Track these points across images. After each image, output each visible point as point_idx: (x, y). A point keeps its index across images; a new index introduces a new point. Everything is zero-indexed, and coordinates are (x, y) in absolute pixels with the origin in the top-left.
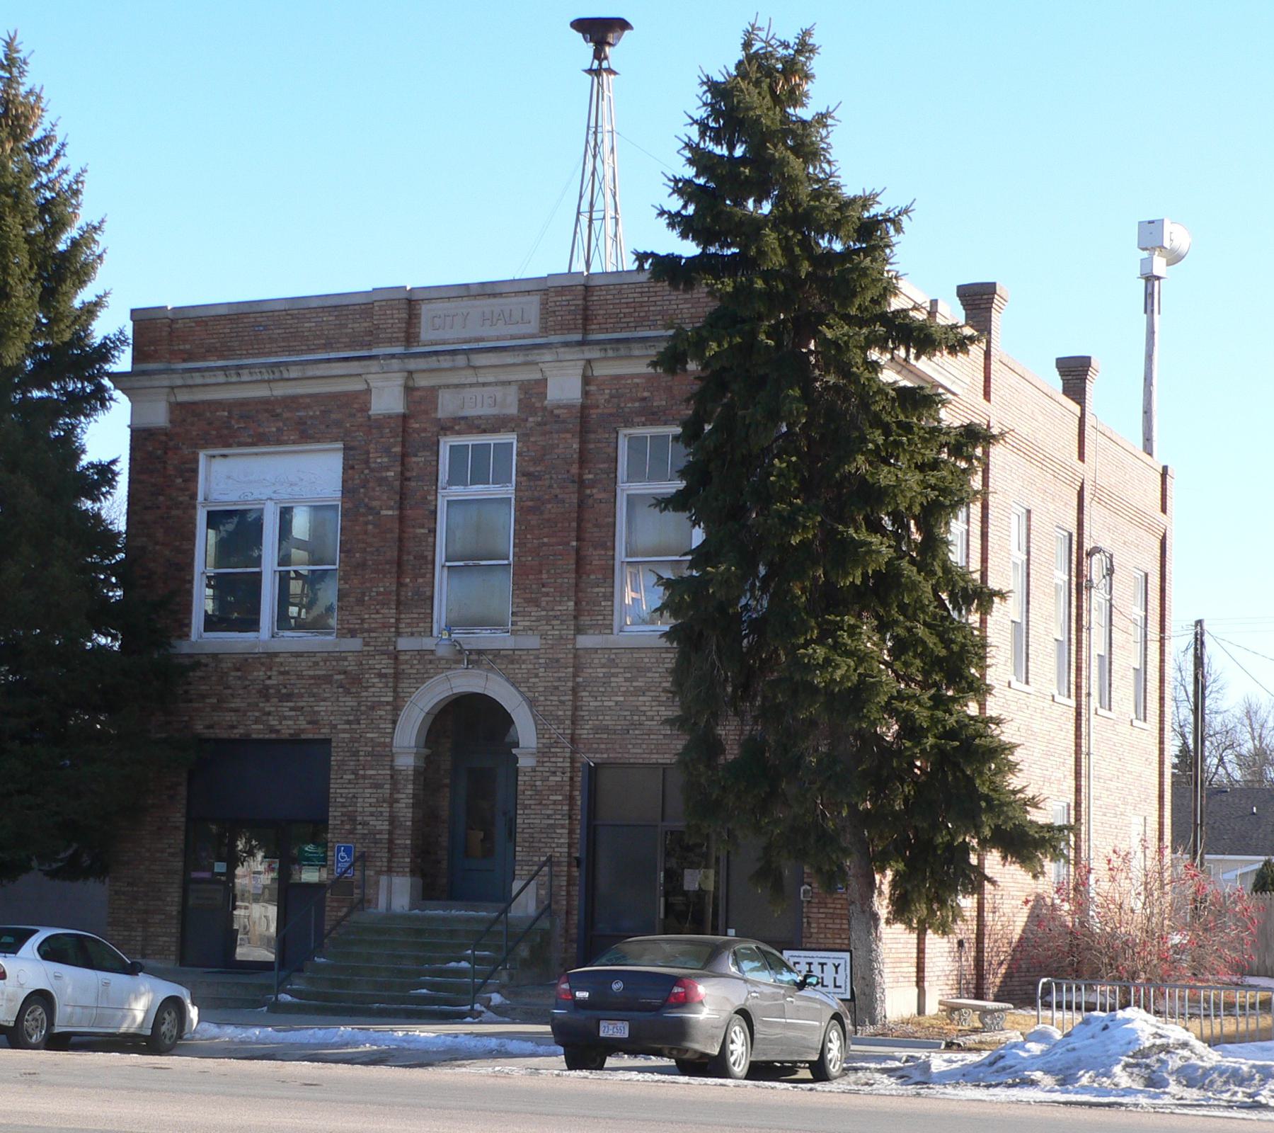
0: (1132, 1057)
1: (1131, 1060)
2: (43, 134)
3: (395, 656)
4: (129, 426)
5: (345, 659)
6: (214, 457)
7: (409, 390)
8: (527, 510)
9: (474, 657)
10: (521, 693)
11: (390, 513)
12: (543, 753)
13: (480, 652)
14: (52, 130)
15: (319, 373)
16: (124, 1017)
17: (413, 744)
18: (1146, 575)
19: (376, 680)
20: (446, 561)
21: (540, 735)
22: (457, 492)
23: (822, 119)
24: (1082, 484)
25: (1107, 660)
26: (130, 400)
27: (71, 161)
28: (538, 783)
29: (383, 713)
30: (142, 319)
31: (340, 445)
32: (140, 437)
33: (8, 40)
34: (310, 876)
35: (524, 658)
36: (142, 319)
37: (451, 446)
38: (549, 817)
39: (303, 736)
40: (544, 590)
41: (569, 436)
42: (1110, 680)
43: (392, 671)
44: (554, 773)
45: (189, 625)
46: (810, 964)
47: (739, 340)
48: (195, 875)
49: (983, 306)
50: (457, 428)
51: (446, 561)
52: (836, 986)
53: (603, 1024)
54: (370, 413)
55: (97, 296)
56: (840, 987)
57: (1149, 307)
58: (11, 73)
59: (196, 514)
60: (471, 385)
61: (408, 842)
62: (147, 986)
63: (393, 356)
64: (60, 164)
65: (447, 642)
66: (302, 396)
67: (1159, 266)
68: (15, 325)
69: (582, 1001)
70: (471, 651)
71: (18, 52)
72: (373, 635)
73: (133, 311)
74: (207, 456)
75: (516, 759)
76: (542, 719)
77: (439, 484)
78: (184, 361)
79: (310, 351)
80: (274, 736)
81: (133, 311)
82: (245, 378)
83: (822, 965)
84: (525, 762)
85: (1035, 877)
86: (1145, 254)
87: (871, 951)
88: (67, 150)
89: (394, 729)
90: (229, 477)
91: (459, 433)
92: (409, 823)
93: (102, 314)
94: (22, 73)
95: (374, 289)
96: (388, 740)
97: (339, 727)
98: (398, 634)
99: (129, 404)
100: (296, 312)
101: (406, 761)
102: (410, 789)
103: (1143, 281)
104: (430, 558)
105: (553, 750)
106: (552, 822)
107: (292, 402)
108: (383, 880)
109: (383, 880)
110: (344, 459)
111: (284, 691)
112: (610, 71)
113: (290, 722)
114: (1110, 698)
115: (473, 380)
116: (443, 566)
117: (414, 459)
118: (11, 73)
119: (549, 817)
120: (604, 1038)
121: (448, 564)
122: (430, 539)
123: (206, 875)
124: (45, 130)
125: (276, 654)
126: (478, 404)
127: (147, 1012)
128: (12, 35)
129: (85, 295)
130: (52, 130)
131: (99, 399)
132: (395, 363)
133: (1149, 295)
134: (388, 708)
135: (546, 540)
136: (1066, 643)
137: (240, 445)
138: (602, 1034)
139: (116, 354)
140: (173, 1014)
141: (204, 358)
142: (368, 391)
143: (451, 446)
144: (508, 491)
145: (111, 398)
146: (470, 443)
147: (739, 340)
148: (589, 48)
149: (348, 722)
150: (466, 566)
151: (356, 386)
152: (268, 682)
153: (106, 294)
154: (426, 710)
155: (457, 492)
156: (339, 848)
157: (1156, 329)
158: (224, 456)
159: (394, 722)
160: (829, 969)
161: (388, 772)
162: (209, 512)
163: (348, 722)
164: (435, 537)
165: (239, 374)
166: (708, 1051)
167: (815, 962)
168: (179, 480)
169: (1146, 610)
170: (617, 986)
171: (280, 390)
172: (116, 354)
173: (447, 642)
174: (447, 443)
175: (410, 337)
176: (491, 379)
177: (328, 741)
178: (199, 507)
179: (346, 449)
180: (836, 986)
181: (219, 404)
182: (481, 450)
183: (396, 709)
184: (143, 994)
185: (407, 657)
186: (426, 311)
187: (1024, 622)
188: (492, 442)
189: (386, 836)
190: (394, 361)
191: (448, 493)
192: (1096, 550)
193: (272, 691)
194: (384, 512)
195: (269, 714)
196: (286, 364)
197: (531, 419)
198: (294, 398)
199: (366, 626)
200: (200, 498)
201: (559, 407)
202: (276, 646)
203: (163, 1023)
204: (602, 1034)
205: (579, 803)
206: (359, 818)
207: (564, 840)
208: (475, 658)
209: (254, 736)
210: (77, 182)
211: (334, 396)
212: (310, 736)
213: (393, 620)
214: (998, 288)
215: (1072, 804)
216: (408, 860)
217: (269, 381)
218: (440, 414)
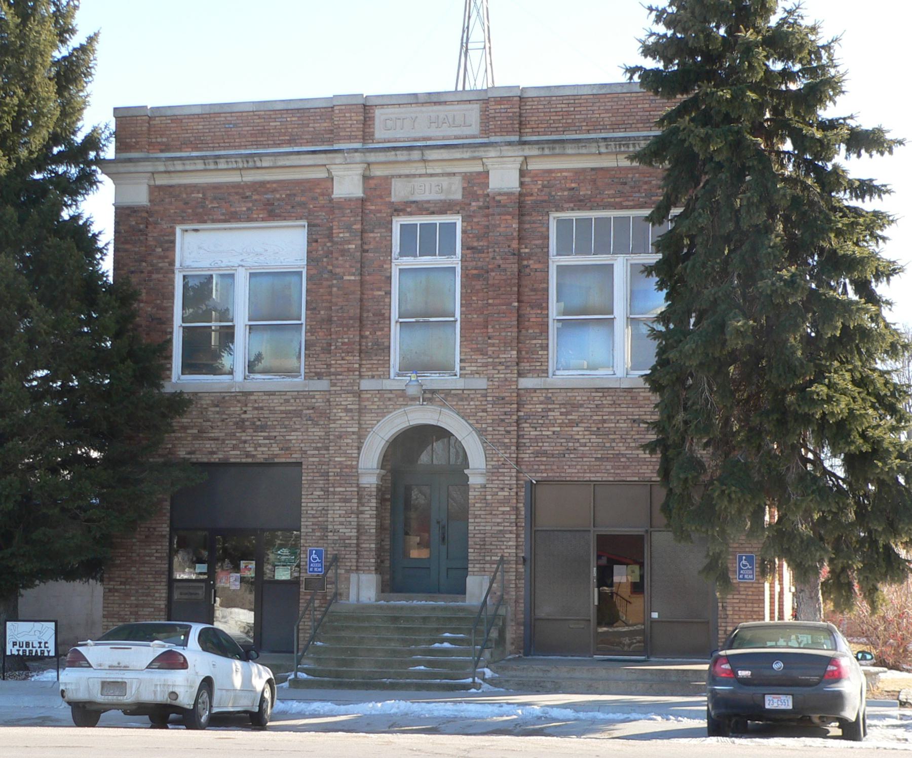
3: (359, 394)
4: (113, 205)
6: (187, 231)
12: (493, 472)
13: (433, 392)
35: (472, 396)
36: (124, 117)
37: (401, 225)
51: (399, 318)
60: (420, 176)
61: (373, 546)
73: (115, 109)
79: (279, 145)
82: (222, 165)
89: (359, 454)
90: (200, 248)
98: (361, 376)
99: (113, 186)
104: (387, 315)
105: (500, 470)
107: (260, 187)
108: (353, 577)
116: (397, 322)
119: (498, 524)
132: (358, 157)
134: (354, 437)
137: (214, 221)
143: (401, 225)
146: (418, 223)
158: (196, 230)
165: (216, 163)
173: (416, 383)
174: (398, 222)
175: (366, 134)
176: (439, 171)
178: (176, 272)
181: (195, 188)
186: (378, 113)
188: (438, 222)
194: (346, 278)
195: (245, 442)
196: (260, 155)
198: (263, 184)
200: (177, 264)
201: (500, 194)
202: (250, 386)
211: (298, 183)
218: (393, 199)
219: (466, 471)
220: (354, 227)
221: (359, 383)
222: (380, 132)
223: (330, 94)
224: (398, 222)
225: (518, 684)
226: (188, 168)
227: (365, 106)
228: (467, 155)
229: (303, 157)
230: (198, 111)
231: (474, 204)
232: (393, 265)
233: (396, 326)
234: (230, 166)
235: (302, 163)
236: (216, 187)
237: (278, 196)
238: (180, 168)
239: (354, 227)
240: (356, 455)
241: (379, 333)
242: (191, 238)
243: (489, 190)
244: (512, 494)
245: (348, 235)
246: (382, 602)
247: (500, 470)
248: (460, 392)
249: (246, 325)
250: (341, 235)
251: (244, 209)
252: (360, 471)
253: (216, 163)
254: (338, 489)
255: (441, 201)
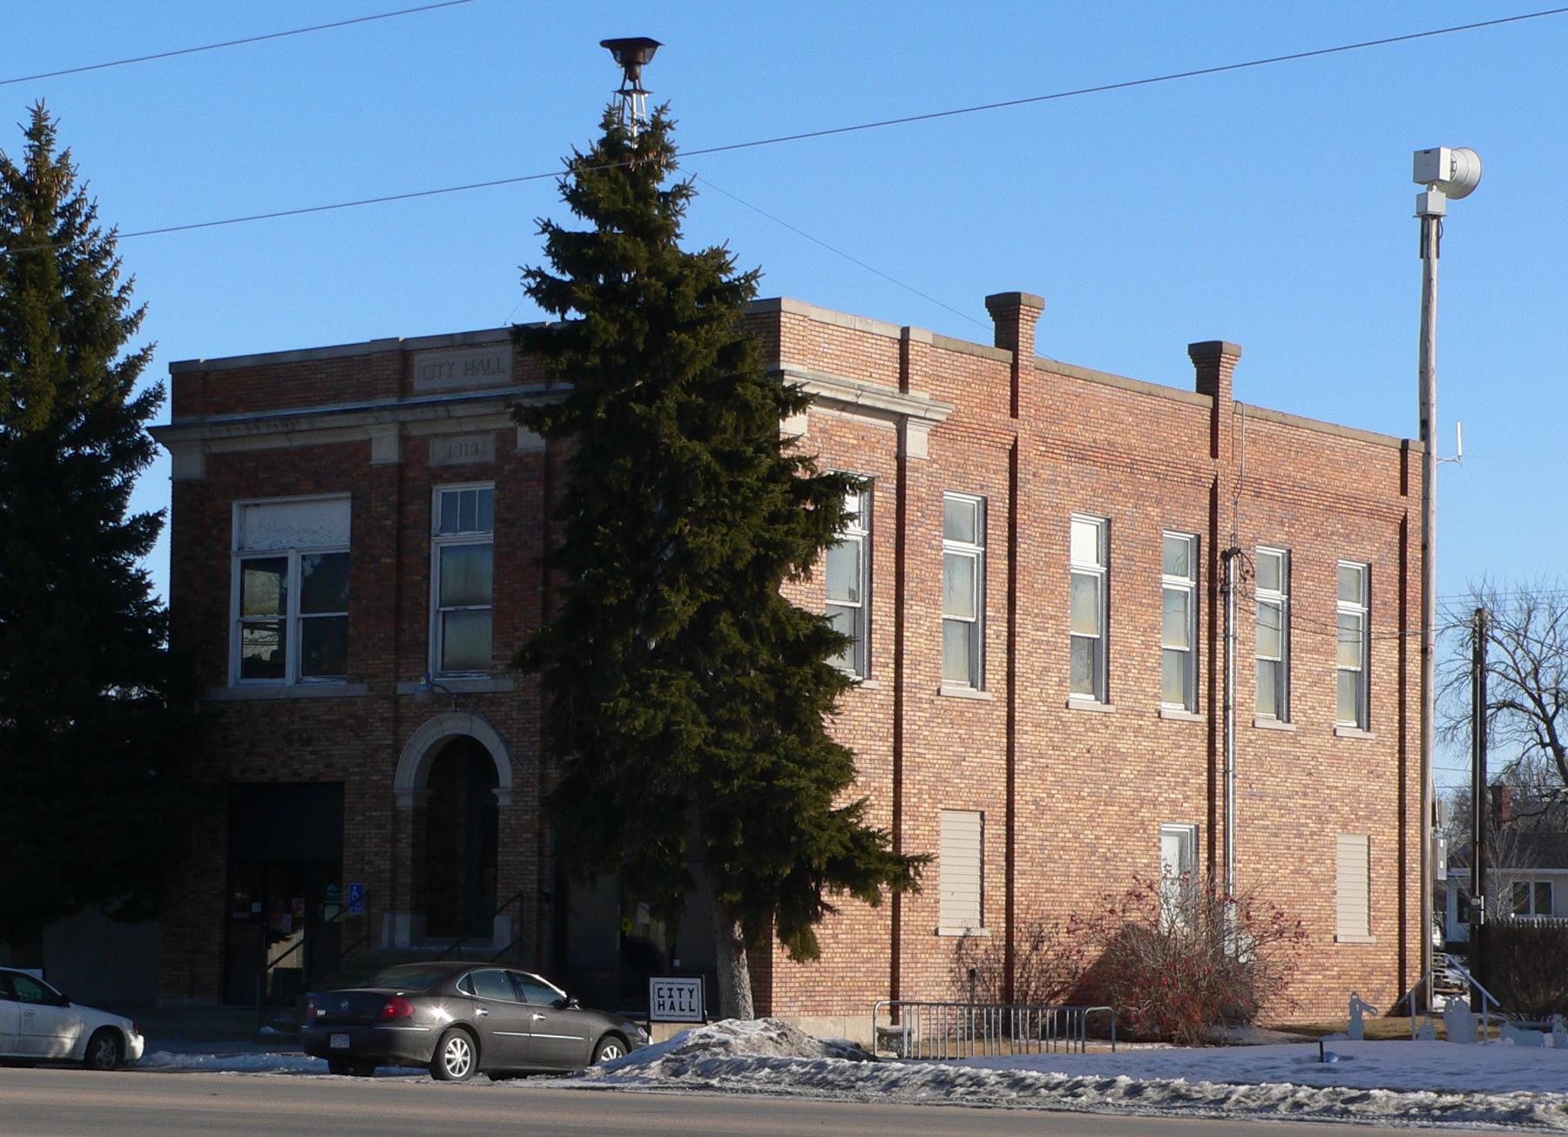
0: (674, 1054)
1: (672, 1056)
2: (74, 198)
3: (396, 700)
4: (170, 478)
5: (354, 704)
6: (247, 506)
7: (404, 439)
8: (503, 554)
9: (461, 700)
10: (500, 735)
11: (388, 560)
12: (517, 792)
13: (467, 695)
14: (82, 194)
15: (325, 425)
16: (50, 1044)
17: (412, 785)
18: (1370, 566)
19: (378, 724)
20: (440, 606)
21: (515, 776)
22: (448, 539)
23: (681, 191)
24: (1216, 480)
25: (1285, 666)
26: (171, 453)
27: (102, 224)
28: (513, 822)
29: (385, 756)
30: (180, 371)
31: (349, 494)
32: (181, 488)
33: (36, 109)
34: (330, 913)
35: (502, 700)
36: (180, 371)
37: (443, 494)
38: (522, 854)
39: (322, 779)
40: (516, 634)
41: (535, 483)
42: (1289, 688)
43: (391, 715)
44: (526, 812)
45: (226, 672)
46: (671, 990)
47: (578, 413)
48: (236, 915)
49: (1011, 317)
50: (445, 476)
51: (440, 606)
52: (691, 1010)
53: (333, 1037)
54: (371, 463)
55: (142, 350)
56: (694, 1010)
57: (1425, 253)
58: (40, 141)
59: (230, 563)
60: (457, 434)
61: (409, 880)
62: (78, 1018)
63: (384, 408)
64: (91, 227)
65: (424, 688)
66: (318, 447)
67: (1437, 202)
68: (34, 394)
69: (321, 1017)
70: (458, 694)
71: (46, 120)
72: (376, 680)
73: (171, 365)
74: (240, 506)
75: (496, 799)
76: (515, 759)
77: (433, 531)
78: (218, 413)
79: (323, 402)
80: (297, 780)
81: (171, 365)
82: (264, 430)
83: (680, 990)
84: (504, 801)
85: (874, 905)
86: (1423, 188)
87: (733, 977)
88: (98, 212)
89: (395, 771)
90: (261, 526)
91: (447, 481)
92: (409, 863)
93: (147, 367)
94: (49, 142)
95: (372, 341)
96: (389, 782)
97: (351, 770)
98: (398, 679)
99: (170, 456)
100: (309, 363)
101: (406, 803)
102: (409, 829)
103: (1419, 220)
104: (424, 604)
105: (525, 790)
106: (524, 859)
107: (307, 452)
108: (387, 917)
109: (387, 917)
110: (352, 507)
111: (305, 735)
112: (642, 92)
113: (310, 766)
114: (1289, 708)
115: (458, 429)
116: (438, 612)
117: (410, 508)
118: (40, 141)
119: (522, 854)
120: (334, 1049)
121: (442, 609)
122: (424, 586)
123: (245, 915)
124: (75, 194)
125: (296, 700)
126: (461, 452)
127: (78, 1041)
128: (40, 104)
129: (126, 350)
130: (82, 194)
131: (142, 453)
132: (387, 415)
133: (1425, 237)
134: (389, 751)
135: (517, 586)
136: (1194, 654)
137: (266, 495)
138: (332, 1045)
139: (153, 409)
140: (111, 1043)
141: (232, 410)
142: (369, 442)
143: (443, 494)
144: (488, 538)
145: (156, 452)
146: (459, 490)
147: (578, 413)
148: (621, 71)
149: (359, 765)
150: (457, 610)
151: (357, 436)
152: (293, 727)
153: (150, 348)
154: (423, 751)
155: (448, 539)
156: (352, 887)
157: (1434, 276)
158: (257, 505)
159: (395, 764)
160: (686, 994)
161: (390, 813)
162: (242, 561)
163: (359, 765)
164: (429, 583)
165: (258, 428)
166: (424, 1060)
167: (675, 987)
168: (215, 531)
169: (1370, 606)
170: (345, 1004)
171: (298, 442)
172: (153, 409)
173: (424, 688)
174: (439, 491)
175: (404, 388)
176: (472, 428)
177: (340, 785)
178: (233, 557)
179: (354, 499)
180: (691, 1010)
181: (247, 455)
182: (468, 496)
183: (397, 751)
184: (73, 1025)
185: (406, 701)
186: (418, 359)
187: (1104, 638)
188: (477, 489)
189: (388, 875)
190: (385, 413)
191: (444, 539)
192: (1235, 551)
193: (295, 736)
194: (383, 560)
195: (293, 758)
196: (297, 417)
197: (507, 467)
198: (310, 448)
199: (370, 671)
200: (234, 547)
201: (527, 456)
202: (299, 692)
203: (99, 1050)
204: (332, 1045)
205: (548, 840)
206: (367, 858)
207: (534, 877)
208: (464, 702)
209: (281, 780)
210: (109, 243)
211: (343, 445)
212: (327, 779)
213: (392, 666)
214: (1022, 298)
215: (1204, 826)
216: (408, 898)
217: (287, 433)
218: (432, 464)
219: (495, 791)
220: (391, 499)
221: (395, 687)
222: (418, 384)
223: (367, 339)
224: (439, 491)
225: (857, 1098)
226: (234, 433)
227: (404, 351)
228: (490, 410)
229: (337, 417)
230: (248, 363)
231: (507, 467)
232: (433, 544)
233: (436, 618)
234: (271, 430)
235: (337, 424)
236: (266, 453)
237: (324, 463)
238: (225, 434)
239: (391, 499)
240: (390, 773)
241: (416, 626)
242: (253, 516)
243: (516, 451)
244: (536, 817)
245: (384, 509)
246: (415, 947)
247: (525, 790)
248: (490, 695)
249: (299, 619)
250: (379, 509)
251: (293, 480)
252: (396, 791)
253: (258, 428)
254: (374, 813)
255: (475, 464)
